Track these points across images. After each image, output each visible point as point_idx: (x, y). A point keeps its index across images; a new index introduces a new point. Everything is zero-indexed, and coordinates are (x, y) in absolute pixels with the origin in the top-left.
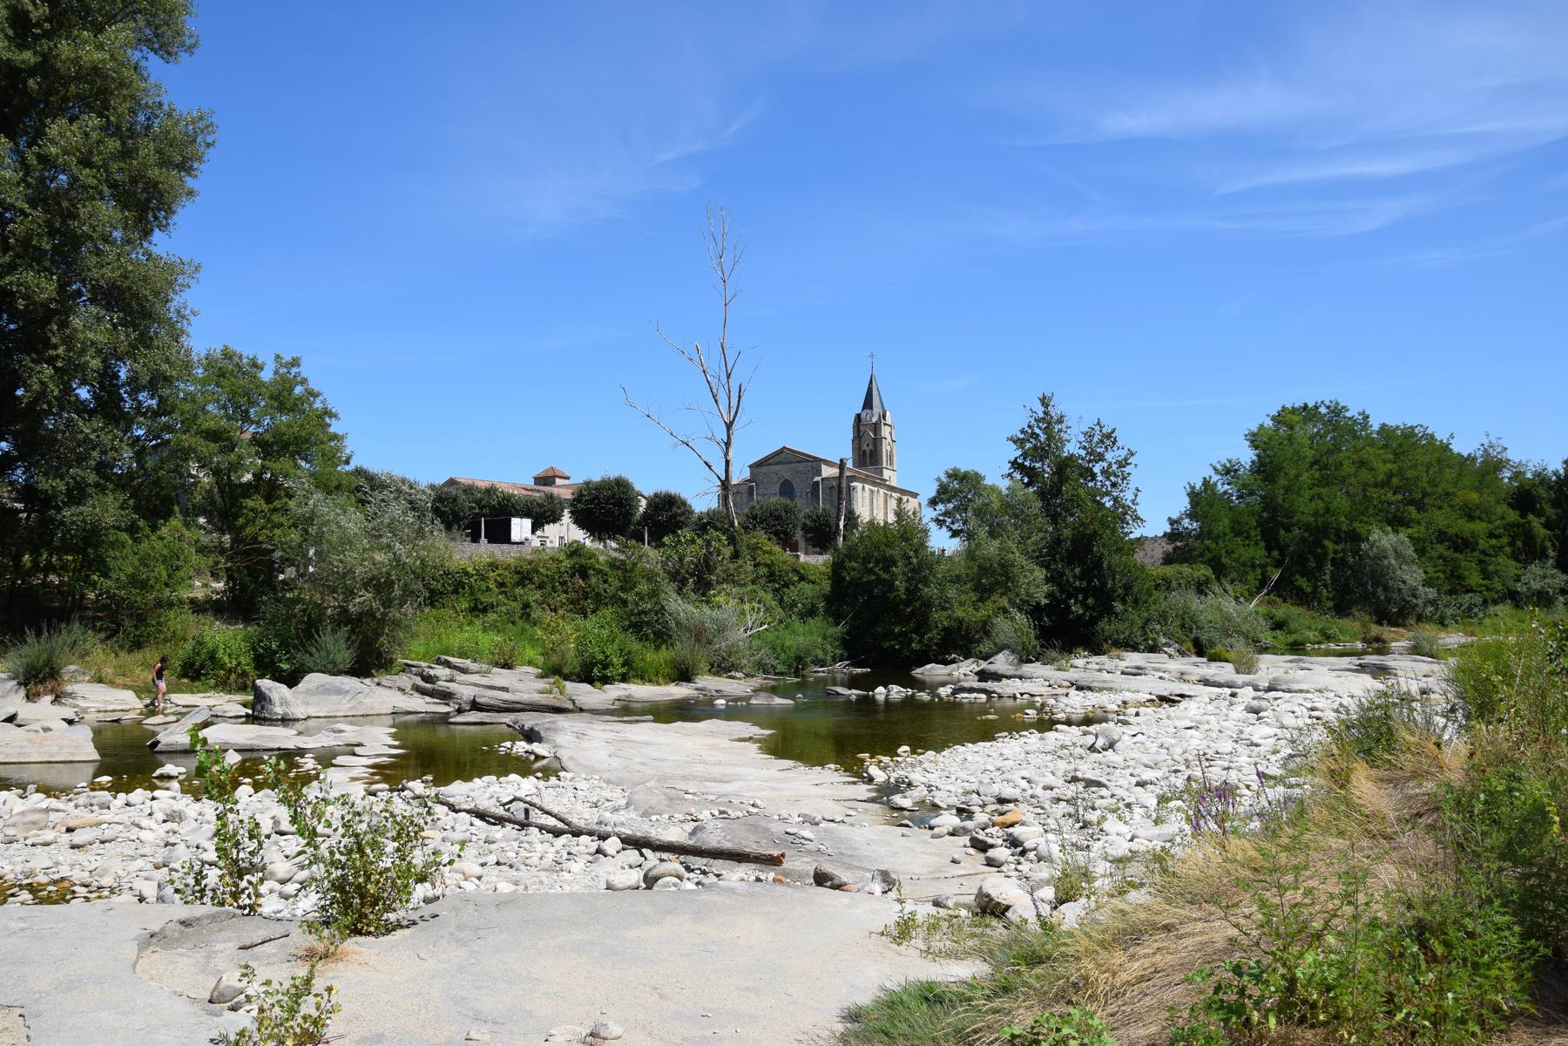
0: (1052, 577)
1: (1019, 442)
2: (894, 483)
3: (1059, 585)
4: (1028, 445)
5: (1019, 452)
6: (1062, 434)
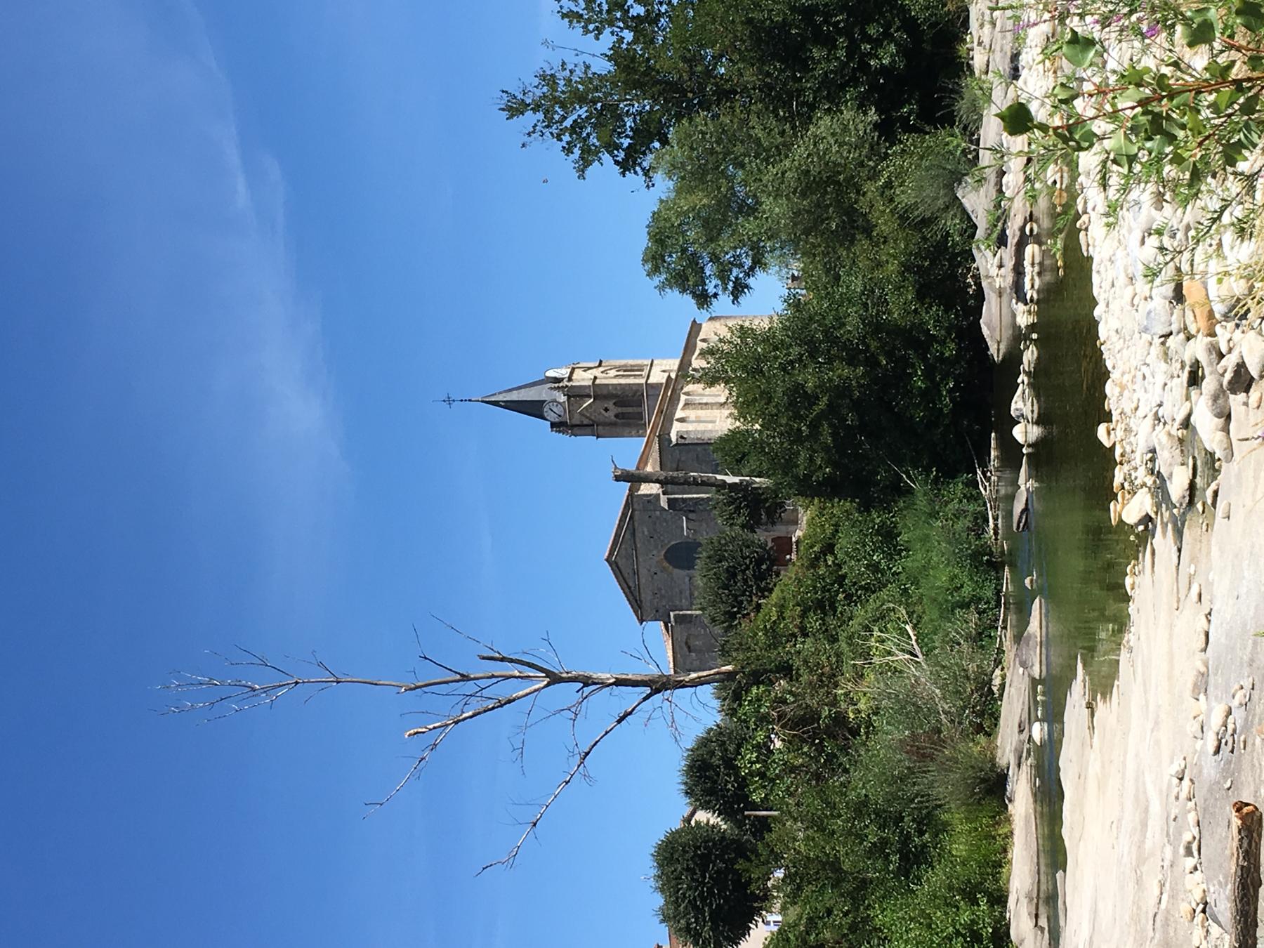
0: (829, 98)
1: (587, 158)
2: (674, 364)
3: (842, 87)
4: (593, 140)
5: (606, 157)
6: (575, 78)
